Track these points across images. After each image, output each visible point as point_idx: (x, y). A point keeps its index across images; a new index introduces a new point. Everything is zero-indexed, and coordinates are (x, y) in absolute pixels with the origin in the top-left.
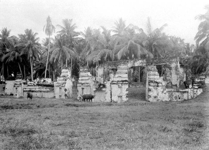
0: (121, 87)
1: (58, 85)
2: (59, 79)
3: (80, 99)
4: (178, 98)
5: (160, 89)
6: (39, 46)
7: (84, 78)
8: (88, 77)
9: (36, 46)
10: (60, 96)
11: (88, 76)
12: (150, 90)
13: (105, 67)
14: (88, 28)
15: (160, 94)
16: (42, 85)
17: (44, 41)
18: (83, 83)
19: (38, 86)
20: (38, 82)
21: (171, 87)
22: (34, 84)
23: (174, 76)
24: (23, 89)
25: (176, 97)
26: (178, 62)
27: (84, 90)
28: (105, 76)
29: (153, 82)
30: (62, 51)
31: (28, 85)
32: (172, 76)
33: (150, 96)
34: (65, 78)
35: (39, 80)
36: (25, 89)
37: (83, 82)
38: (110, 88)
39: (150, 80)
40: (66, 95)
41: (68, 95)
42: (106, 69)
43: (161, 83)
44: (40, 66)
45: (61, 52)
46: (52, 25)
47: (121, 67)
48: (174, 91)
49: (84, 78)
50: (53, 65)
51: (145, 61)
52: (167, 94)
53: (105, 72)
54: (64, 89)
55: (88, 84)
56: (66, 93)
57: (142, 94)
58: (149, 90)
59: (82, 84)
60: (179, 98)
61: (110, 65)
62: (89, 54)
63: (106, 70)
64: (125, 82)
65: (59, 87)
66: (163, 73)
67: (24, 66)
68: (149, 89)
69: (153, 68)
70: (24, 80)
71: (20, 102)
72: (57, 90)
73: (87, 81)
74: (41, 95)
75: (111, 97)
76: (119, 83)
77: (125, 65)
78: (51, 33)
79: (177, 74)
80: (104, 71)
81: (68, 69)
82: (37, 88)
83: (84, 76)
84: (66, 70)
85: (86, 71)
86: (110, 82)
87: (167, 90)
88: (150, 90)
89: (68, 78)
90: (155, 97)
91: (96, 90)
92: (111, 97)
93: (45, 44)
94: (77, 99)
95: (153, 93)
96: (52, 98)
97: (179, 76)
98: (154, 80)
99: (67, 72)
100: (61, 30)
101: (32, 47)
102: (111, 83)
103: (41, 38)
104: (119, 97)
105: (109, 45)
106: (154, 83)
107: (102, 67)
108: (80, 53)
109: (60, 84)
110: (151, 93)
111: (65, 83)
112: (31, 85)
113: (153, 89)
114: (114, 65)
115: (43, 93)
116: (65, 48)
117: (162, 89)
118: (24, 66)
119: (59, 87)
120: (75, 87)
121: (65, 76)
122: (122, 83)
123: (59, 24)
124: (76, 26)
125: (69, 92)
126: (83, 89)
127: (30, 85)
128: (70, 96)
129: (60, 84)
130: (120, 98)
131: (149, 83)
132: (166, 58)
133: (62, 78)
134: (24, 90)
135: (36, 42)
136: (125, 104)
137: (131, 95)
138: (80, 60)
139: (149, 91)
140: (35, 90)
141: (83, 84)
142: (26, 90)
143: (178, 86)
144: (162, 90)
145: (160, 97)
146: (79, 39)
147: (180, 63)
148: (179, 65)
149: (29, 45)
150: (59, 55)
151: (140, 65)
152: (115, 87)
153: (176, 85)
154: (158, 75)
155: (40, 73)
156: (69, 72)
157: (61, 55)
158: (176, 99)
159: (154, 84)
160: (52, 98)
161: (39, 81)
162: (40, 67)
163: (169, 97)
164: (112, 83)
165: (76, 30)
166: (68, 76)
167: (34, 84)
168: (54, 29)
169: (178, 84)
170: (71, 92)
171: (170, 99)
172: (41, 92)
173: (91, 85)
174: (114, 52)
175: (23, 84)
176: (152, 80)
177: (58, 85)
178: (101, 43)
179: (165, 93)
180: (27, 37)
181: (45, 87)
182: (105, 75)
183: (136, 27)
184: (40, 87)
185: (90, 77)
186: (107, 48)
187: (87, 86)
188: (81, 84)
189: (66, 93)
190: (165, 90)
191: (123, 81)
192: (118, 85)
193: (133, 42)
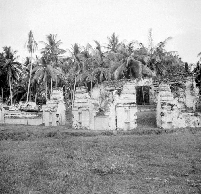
0: (128, 111)
1: (47, 109)
2: (49, 102)
3: (76, 127)
4: (197, 123)
5: (175, 113)
6: (19, 65)
7: (80, 101)
8: (87, 99)
9: (15, 66)
10: (51, 123)
11: (86, 98)
12: (162, 114)
13: (101, 88)
14: (75, 45)
15: (175, 119)
16: (25, 110)
17: (24, 60)
18: (79, 106)
19: (20, 111)
20: (21, 107)
21: (185, 111)
22: (16, 109)
23: (188, 98)
24: (4, 115)
25: (194, 122)
26: (194, 80)
27: (82, 115)
28: (101, 99)
29: (167, 104)
30: (46, 71)
31: (10, 111)
32: (187, 97)
33: (162, 122)
34: (56, 100)
35: (22, 104)
36: (7, 115)
37: (79, 105)
38: (114, 112)
39: (162, 101)
40: (57, 122)
41: (60, 122)
42: (103, 89)
43: (176, 106)
44: (19, 89)
45: (45, 72)
46: (35, 41)
47: (127, 86)
48: (191, 115)
49: (80, 101)
50: (35, 88)
51: (152, 80)
52: (184, 120)
53: (101, 93)
54: (56, 115)
55: (86, 108)
56: (58, 119)
57: (151, 119)
58: (161, 114)
59: (79, 108)
60: (198, 124)
61: (108, 85)
62: (79, 74)
63: (102, 91)
64: (132, 105)
65: (49, 112)
66: (145, 101)
67: (2, 89)
68: (162, 113)
69: (166, 88)
70: (5, 104)
71: (4, 130)
72: (46, 116)
73: (85, 105)
74: (27, 121)
75: (116, 124)
76: (125, 106)
77: (131, 84)
78: (33, 50)
79: (193, 95)
80: (100, 93)
81: (60, 90)
82: (21, 114)
83: (81, 99)
84: (58, 91)
85: (83, 91)
86: (115, 104)
87: (183, 114)
88: (162, 114)
89: (61, 101)
90: (169, 123)
91: (97, 115)
92: (116, 124)
93: (26, 64)
94: (73, 126)
95: (166, 119)
96: (42, 124)
97: (194, 97)
98: (167, 102)
99: (59, 93)
100: (44, 46)
101: (12, 66)
102: (116, 106)
103: (21, 56)
104: (126, 123)
105: (104, 63)
106: (168, 105)
107: (98, 87)
108: (66, 73)
109: (50, 109)
110: (164, 118)
111: (57, 107)
112: (12, 110)
113: (167, 113)
114: (113, 85)
115: (28, 119)
116: (50, 67)
117: (178, 113)
118: (2, 89)
119: (49, 112)
120: (68, 113)
121: (56, 99)
122: (130, 106)
123: (42, 41)
124: (62, 42)
125: (62, 118)
126: (80, 113)
127: (11, 111)
128: (63, 123)
129: (50, 109)
130: (127, 124)
131: (162, 105)
132: (179, 76)
133: (53, 101)
134: (6, 116)
135: (15, 61)
136: (133, 132)
137: (140, 121)
138: (66, 82)
139: (162, 115)
140: (19, 116)
141: (80, 107)
142: (8, 116)
143: (194, 109)
144: (177, 115)
145: (175, 123)
146: (64, 58)
147: (196, 81)
148: (195, 83)
149: (8, 64)
150: (44, 76)
151: (145, 85)
152: (120, 111)
153: (192, 108)
154: (171, 96)
155: (20, 97)
156: (61, 94)
157: (45, 76)
158: (194, 125)
159: (168, 107)
160: (40, 125)
161: (22, 105)
162: (19, 90)
163: (186, 123)
164: (118, 106)
165: (61, 47)
166: (60, 98)
167: (16, 109)
168: (37, 45)
169: (194, 107)
170: (64, 118)
171: (187, 126)
172: (26, 118)
173: (90, 109)
174: (110, 71)
175: (3, 109)
176: (165, 102)
177: (47, 109)
178: (94, 60)
179: (181, 118)
180: (5, 55)
181: (29, 113)
182: (102, 98)
183: (135, 42)
184: (23, 112)
185: (88, 99)
186: (101, 65)
187: (85, 110)
188: (78, 108)
189: (58, 119)
190: (181, 114)
191: (130, 104)
192: (125, 109)
193: (133, 58)
